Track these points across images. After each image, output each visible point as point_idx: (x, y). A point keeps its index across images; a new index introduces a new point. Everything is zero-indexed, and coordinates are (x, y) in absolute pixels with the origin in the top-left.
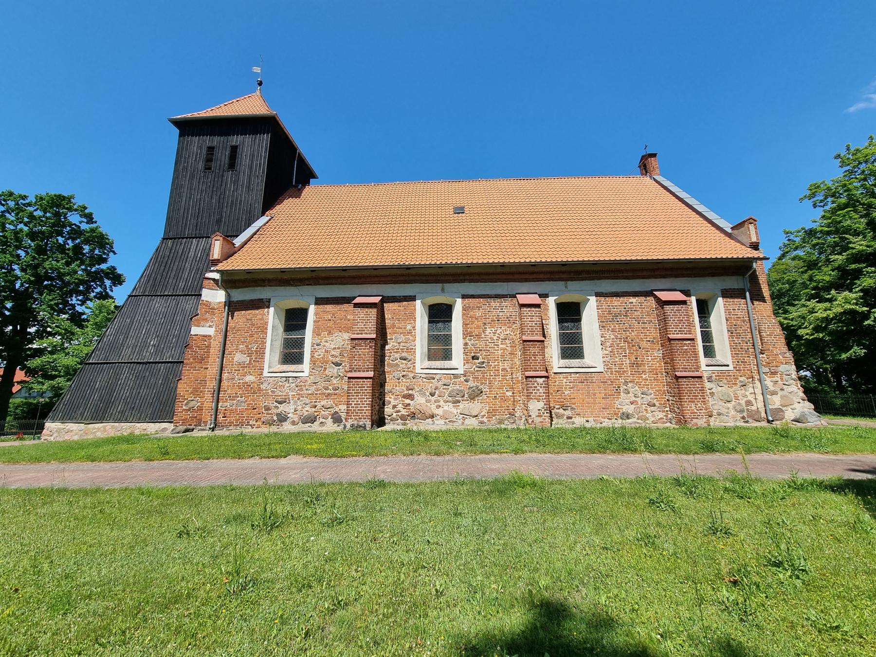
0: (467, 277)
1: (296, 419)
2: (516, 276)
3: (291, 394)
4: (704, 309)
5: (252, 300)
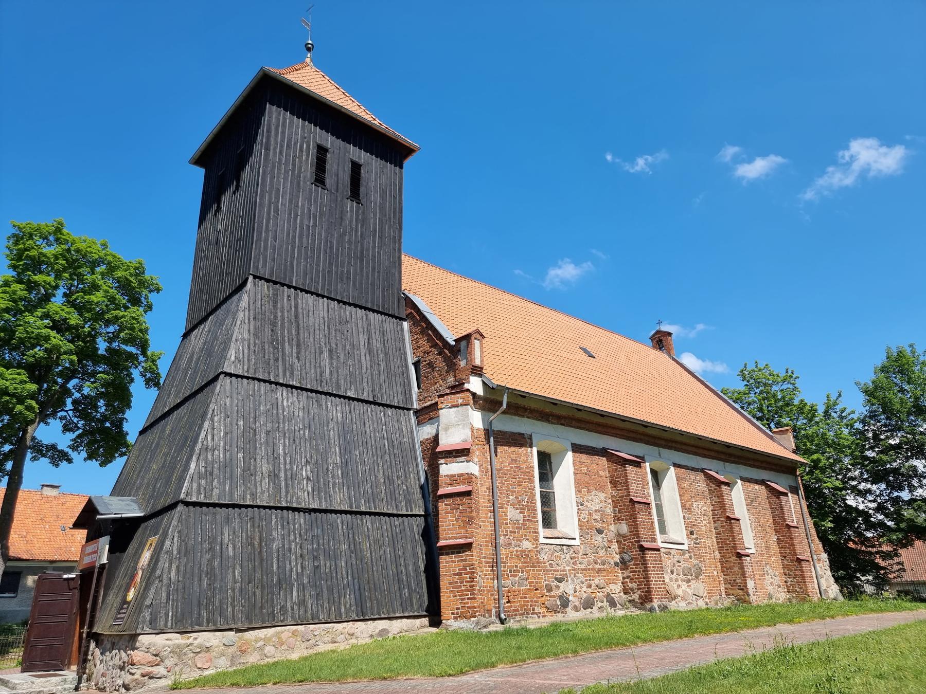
0: (674, 445)
1: (577, 604)
2: (701, 451)
3: (567, 568)
4: (546, 463)
5: (513, 434)
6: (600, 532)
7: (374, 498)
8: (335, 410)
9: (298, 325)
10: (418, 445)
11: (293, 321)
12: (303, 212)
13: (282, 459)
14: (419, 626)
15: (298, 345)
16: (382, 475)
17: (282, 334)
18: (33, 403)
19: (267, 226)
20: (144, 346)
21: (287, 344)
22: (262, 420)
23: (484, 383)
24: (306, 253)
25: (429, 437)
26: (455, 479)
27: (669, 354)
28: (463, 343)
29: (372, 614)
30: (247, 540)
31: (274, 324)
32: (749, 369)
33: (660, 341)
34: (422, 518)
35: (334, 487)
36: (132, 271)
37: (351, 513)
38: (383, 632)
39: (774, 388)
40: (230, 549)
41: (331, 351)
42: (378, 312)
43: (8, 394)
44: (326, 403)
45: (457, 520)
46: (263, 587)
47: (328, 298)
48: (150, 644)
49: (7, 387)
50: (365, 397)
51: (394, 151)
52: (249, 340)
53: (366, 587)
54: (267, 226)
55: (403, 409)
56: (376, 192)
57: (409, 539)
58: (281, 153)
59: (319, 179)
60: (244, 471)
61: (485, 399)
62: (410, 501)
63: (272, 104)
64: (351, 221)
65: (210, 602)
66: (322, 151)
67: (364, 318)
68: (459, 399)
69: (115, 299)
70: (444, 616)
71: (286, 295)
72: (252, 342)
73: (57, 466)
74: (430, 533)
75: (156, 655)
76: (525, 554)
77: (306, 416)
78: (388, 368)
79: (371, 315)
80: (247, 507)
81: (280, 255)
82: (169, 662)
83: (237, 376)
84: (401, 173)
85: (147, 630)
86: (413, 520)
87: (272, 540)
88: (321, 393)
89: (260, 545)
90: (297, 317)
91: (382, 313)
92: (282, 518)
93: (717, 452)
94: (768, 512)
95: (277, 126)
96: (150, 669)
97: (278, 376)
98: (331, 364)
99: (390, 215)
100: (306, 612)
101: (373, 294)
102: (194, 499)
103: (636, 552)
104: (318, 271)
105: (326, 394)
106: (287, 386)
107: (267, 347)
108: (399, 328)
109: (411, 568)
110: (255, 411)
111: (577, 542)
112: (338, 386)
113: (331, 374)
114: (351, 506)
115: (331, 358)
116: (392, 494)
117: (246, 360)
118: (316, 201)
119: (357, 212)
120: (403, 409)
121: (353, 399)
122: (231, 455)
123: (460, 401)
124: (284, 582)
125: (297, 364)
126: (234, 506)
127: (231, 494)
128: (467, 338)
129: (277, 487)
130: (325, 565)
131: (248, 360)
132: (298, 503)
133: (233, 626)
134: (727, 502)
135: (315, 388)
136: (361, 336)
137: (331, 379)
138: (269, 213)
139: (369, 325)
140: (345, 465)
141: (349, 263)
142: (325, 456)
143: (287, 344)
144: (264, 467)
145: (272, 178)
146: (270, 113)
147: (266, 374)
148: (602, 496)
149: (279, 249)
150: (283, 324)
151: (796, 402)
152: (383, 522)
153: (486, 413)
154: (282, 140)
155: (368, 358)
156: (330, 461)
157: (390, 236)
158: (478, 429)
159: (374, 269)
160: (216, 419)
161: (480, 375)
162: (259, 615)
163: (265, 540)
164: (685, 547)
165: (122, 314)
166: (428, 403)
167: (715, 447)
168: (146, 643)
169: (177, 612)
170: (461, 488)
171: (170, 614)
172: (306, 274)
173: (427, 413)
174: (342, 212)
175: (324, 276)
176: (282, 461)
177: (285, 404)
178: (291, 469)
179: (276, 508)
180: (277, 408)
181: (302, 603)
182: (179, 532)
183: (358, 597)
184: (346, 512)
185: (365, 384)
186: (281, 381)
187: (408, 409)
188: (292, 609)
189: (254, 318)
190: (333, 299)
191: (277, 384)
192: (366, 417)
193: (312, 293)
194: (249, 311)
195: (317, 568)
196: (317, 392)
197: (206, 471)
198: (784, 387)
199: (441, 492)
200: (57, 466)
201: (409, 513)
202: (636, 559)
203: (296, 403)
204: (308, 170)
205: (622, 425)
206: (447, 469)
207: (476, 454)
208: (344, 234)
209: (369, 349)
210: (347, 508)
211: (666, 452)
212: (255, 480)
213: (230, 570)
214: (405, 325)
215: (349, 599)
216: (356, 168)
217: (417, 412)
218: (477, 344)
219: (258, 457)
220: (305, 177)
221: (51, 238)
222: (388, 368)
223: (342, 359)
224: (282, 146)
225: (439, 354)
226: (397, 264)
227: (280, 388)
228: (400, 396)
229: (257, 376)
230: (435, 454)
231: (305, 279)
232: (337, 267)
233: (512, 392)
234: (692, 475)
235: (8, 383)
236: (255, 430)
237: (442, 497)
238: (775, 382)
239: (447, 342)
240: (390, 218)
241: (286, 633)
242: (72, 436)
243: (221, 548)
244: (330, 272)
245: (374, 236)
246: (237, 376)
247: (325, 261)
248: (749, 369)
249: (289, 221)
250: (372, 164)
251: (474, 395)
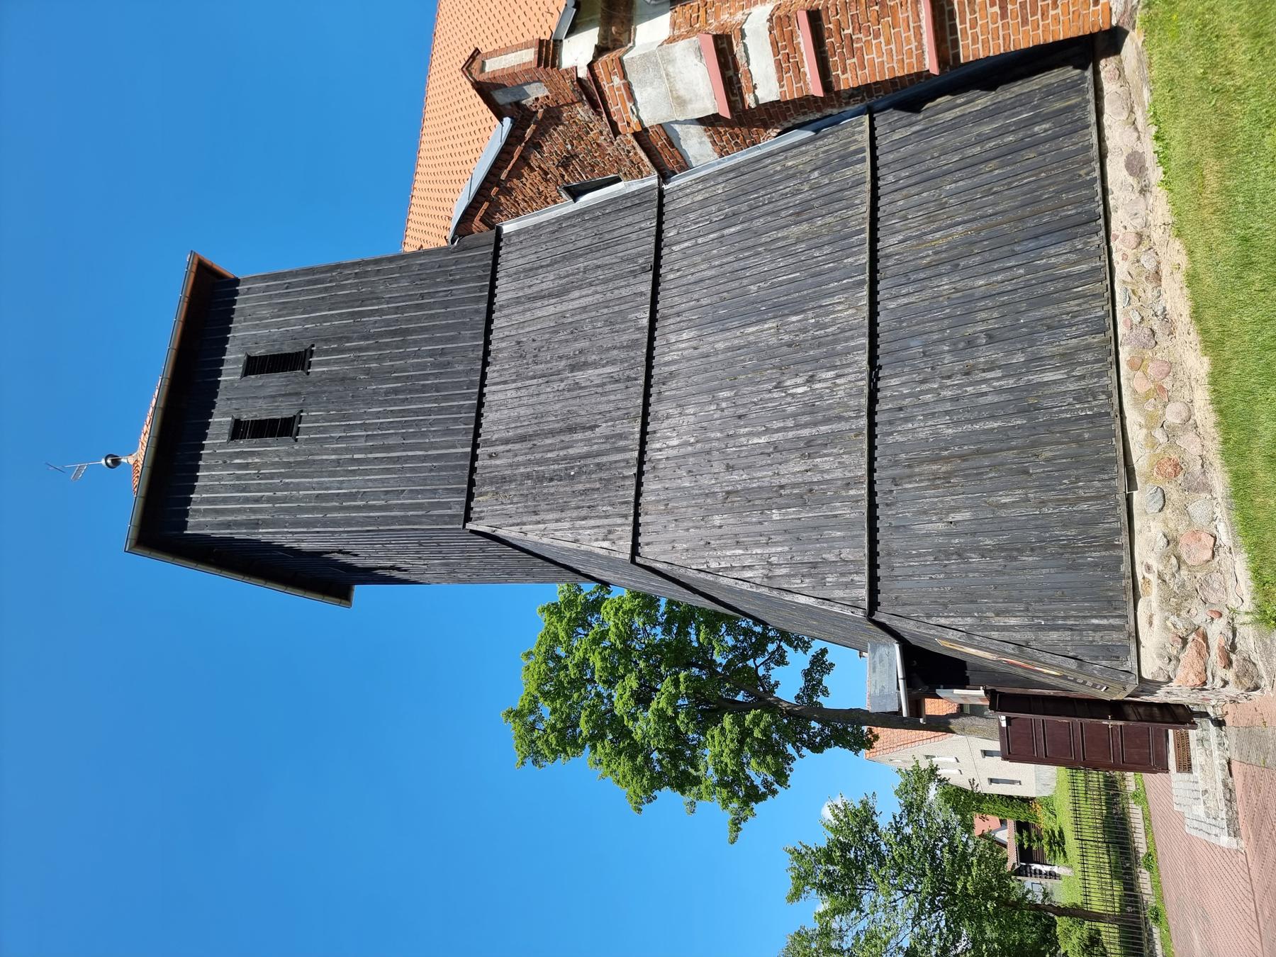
7: (840, 239)
8: (677, 345)
9: (536, 435)
10: (729, 162)
11: (529, 445)
12: (347, 450)
13: (776, 437)
14: (1125, 80)
15: (571, 430)
16: (794, 229)
17: (555, 461)
18: (749, 717)
19: (380, 508)
21: (571, 451)
22: (706, 481)
23: (572, 31)
24: (414, 435)
25: (707, 140)
26: (786, 63)
28: (501, 98)
29: (1092, 199)
30: (937, 487)
31: (540, 479)
34: (879, 118)
35: (825, 326)
36: (554, 619)
37: (874, 283)
38: (1135, 165)
40: (958, 517)
41: (573, 368)
42: (493, 287)
44: (667, 364)
45: (877, 36)
46: (1034, 445)
47: (483, 385)
48: (1161, 656)
49: (732, 751)
50: (647, 288)
51: (211, 298)
52: (572, 519)
53: (1031, 223)
54: (380, 508)
55: (661, 206)
56: (288, 323)
57: (923, 145)
58: (257, 500)
59: (283, 428)
60: (804, 504)
61: (606, 23)
62: (843, 158)
63: (184, 525)
64: (345, 361)
65: (1069, 546)
66: (240, 430)
67: (506, 312)
68: (612, 85)
69: (594, 639)
70: (1101, 24)
71: (488, 462)
72: (575, 514)
73: (832, 665)
74: (908, 95)
75: (1185, 641)
77: (693, 400)
78: (590, 250)
79: (500, 299)
80: (872, 494)
81: (424, 481)
82: (1200, 616)
83: (636, 534)
84: (247, 280)
85: (1131, 664)
86: (882, 143)
87: (936, 434)
88: (648, 376)
89: (947, 460)
90: (523, 439)
91: (494, 279)
92: (890, 423)
95: (217, 512)
96: (1215, 651)
97: (627, 461)
98: (595, 365)
99: (320, 291)
100: (1088, 348)
101: (462, 302)
102: (864, 593)
104: (441, 410)
105: (649, 367)
106: (643, 443)
107: (580, 487)
108: (515, 240)
109: (986, 129)
110: (694, 497)
112: (633, 345)
113: (612, 362)
114: (860, 284)
115: (586, 365)
116: (832, 199)
117: (606, 522)
118: (325, 430)
119: (327, 352)
120: (661, 206)
121: (653, 311)
122: (776, 532)
123: (617, 81)
124: (1025, 402)
125: (604, 429)
126: (872, 518)
127: (850, 524)
128: (485, 90)
129: (830, 440)
130: (986, 320)
131: (607, 517)
132: (860, 394)
133: (1121, 498)
135: (642, 390)
136: (539, 313)
137: (622, 361)
138: (358, 508)
139: (517, 301)
140: (779, 310)
141: (416, 355)
142: (767, 353)
143: (571, 451)
144: (793, 469)
145: (301, 510)
146: (198, 525)
147: (628, 483)
149: (415, 484)
150: (539, 462)
152: (889, 209)
153: (638, 11)
154: (237, 500)
155: (576, 294)
156: (773, 341)
157: (356, 285)
158: (674, 24)
159: (419, 307)
160: (714, 565)
161: (557, 43)
162: (1097, 449)
163: (937, 451)
165: (613, 629)
166: (642, 154)
168: (1159, 663)
169: (1092, 609)
170: (804, 39)
171: (1095, 621)
172: (448, 432)
173: (659, 150)
174: (332, 380)
175: (446, 398)
176: (780, 436)
177: (675, 442)
178: (794, 416)
179: (872, 436)
180: (684, 456)
181: (1068, 359)
182: (929, 616)
183: (1053, 239)
184: (873, 293)
185: (624, 292)
186: (636, 454)
187: (661, 194)
188: (1083, 377)
189: (536, 513)
190: (484, 376)
191: (641, 462)
192: (684, 281)
193: (479, 415)
194: (524, 524)
195: (991, 337)
196: (648, 385)
197: (810, 575)
199: (816, 90)
200: (832, 665)
201: (867, 154)
203: (672, 421)
204: (275, 448)
206: (765, 84)
207: (726, 18)
208: (368, 371)
209: (561, 293)
210: (865, 292)
212: (819, 482)
213: (1003, 513)
214: (508, 227)
215: (1058, 257)
216: (254, 366)
217: (664, 176)
218: (494, 66)
219: (776, 482)
220: (289, 454)
221: (531, 718)
222: (590, 250)
223: (584, 344)
224: (247, 500)
225: (538, 147)
226: (402, 263)
227: (650, 455)
228: (637, 218)
229: (632, 499)
230: (739, 119)
231: (457, 432)
232: (426, 377)
235: (727, 751)
236: (728, 493)
239: (511, 134)
240: (326, 289)
241: (1135, 384)
243: (957, 535)
244: (437, 388)
245: (362, 314)
246: (636, 534)
247: (421, 400)
249: (366, 472)
250: (244, 338)
251: (600, 50)
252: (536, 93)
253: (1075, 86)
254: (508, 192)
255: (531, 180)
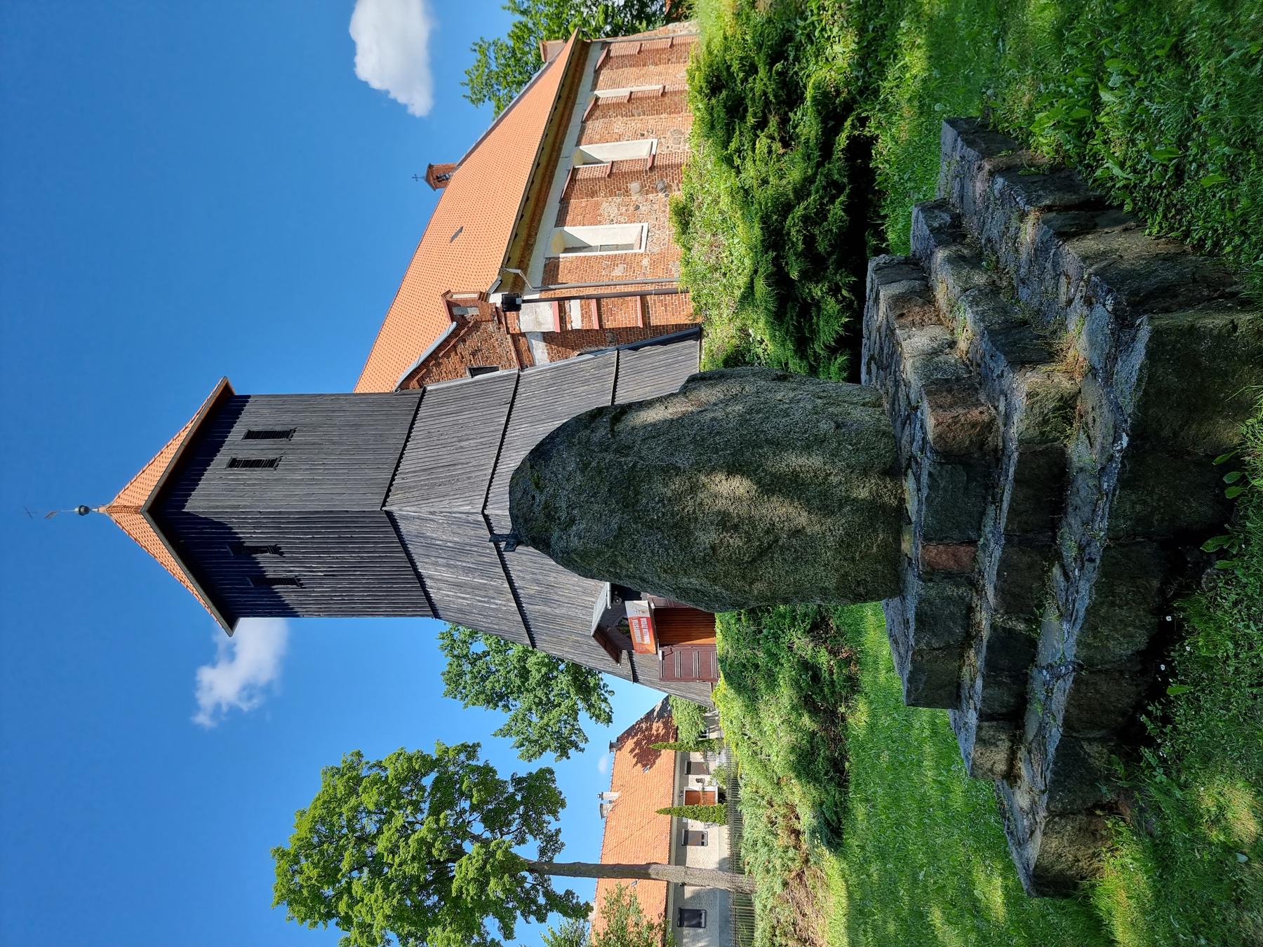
2: (564, 123)
6: (637, 208)
10: (553, 365)
20: (430, 764)
23: (496, 291)
27: (453, 169)
28: (456, 311)
32: (469, 93)
33: (437, 178)
39: (494, 68)
43: (484, 867)
51: (228, 406)
59: (271, 464)
63: (184, 507)
66: (234, 463)
73: (563, 844)
76: (653, 264)
93: (565, 108)
94: (626, 70)
103: (655, 175)
111: (646, 225)
128: (450, 305)
134: (614, 101)
148: (605, 205)
151: (511, 43)
161: (488, 295)
164: (655, 141)
167: (560, 109)
193: (399, 462)
198: (493, 55)
200: (563, 844)
202: (662, 176)
205: (537, 181)
211: (564, 152)
216: (251, 435)
217: (522, 368)
225: (464, 341)
233: (507, 261)
234: (588, 131)
237: (601, 326)
238: (488, 66)
242: (529, 837)
248: (469, 93)
252: (472, 313)
253: (693, 346)
254: (438, 365)
255: (454, 358)
